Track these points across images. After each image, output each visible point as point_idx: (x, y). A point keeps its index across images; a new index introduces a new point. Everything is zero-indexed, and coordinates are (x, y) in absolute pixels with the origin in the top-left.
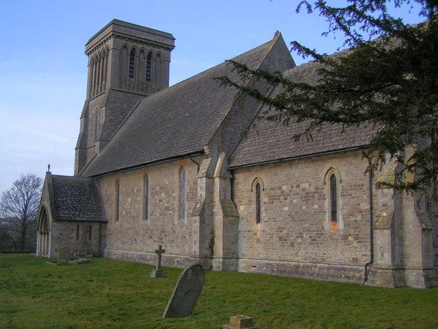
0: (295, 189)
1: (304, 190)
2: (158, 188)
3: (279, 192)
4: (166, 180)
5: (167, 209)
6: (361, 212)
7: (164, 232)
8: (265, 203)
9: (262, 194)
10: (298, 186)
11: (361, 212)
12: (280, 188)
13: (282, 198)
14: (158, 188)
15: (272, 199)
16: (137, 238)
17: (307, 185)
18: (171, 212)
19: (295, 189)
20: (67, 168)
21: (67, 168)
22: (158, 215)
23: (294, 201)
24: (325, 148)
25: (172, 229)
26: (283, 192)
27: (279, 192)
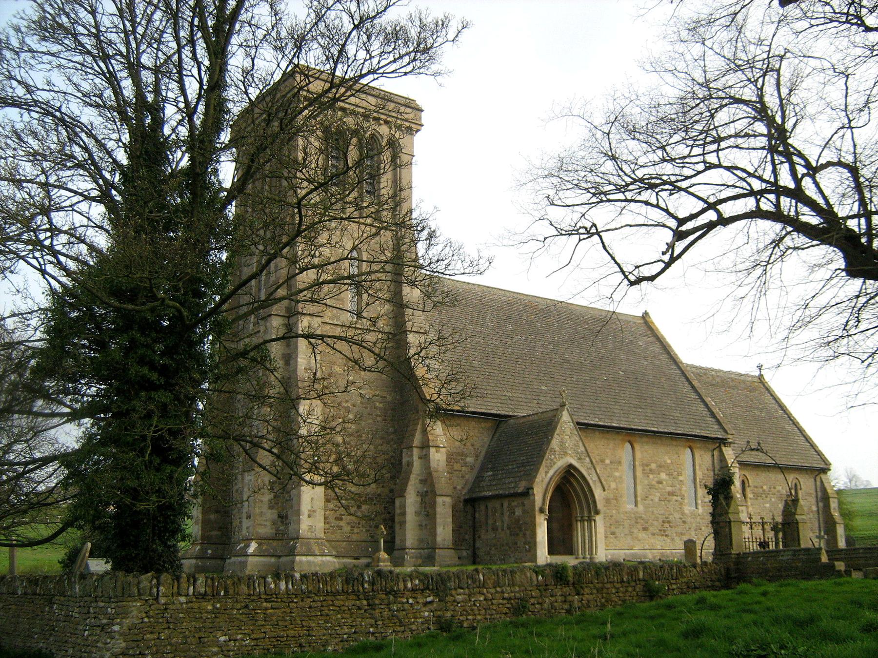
0: (772, 489)
1: (779, 491)
2: (653, 466)
3: (761, 490)
4: (666, 457)
5: (671, 494)
6: (812, 512)
7: (669, 522)
8: (750, 499)
9: (748, 490)
10: (774, 488)
11: (812, 512)
12: (762, 487)
13: (764, 496)
14: (653, 466)
15: (757, 496)
16: (617, 530)
17: (780, 488)
18: (679, 498)
19: (772, 489)
20: (790, 141)
21: (790, 141)
22: (656, 500)
23: (773, 500)
24: (606, 480)
25: (681, 518)
26: (764, 491)
27: (761, 490)
